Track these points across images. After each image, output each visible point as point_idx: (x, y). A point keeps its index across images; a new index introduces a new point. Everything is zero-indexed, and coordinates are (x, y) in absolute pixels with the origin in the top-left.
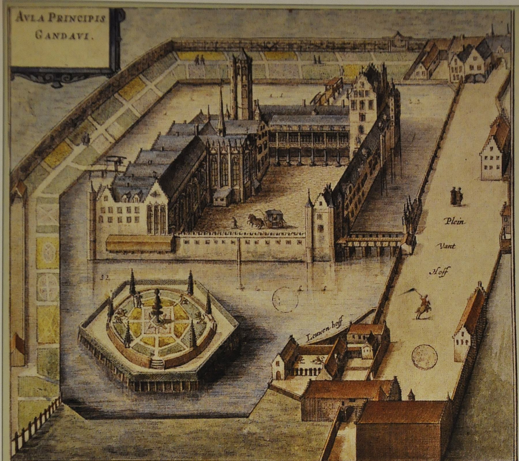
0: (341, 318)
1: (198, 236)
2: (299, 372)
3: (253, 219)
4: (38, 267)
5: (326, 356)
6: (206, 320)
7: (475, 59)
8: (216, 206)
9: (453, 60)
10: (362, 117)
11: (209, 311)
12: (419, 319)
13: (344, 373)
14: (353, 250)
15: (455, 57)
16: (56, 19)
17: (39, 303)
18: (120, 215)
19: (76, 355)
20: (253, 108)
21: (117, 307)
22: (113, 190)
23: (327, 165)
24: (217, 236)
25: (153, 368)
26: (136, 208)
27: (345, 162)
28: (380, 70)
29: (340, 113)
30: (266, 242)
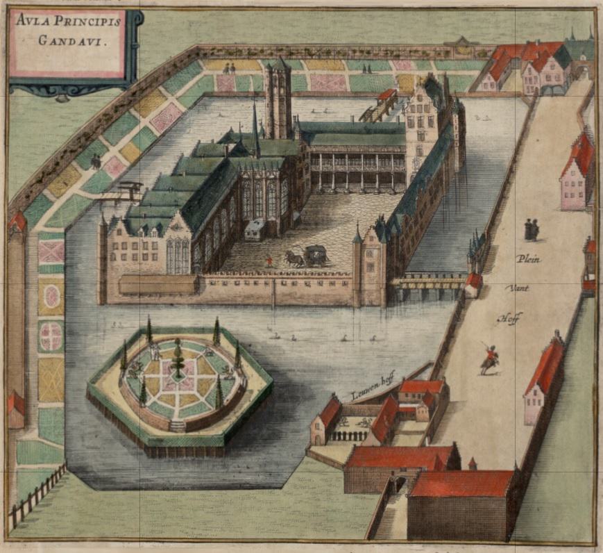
0: (392, 373)
1: (225, 276)
2: (342, 437)
3: (291, 258)
4: (40, 314)
5: (374, 419)
6: (235, 375)
7: (552, 67)
8: (247, 242)
9: (527, 70)
10: (421, 137)
11: (238, 365)
12: (484, 375)
13: (395, 438)
14: (407, 292)
15: (529, 66)
16: (63, 22)
17: (41, 356)
18: (135, 252)
19: (86, 414)
20: (293, 127)
21: (132, 360)
22: (127, 223)
23: (379, 193)
24: (248, 276)
25: (172, 431)
26: (153, 243)
27: (401, 189)
28: (441, 81)
29: (393, 132)
30: (306, 284)
